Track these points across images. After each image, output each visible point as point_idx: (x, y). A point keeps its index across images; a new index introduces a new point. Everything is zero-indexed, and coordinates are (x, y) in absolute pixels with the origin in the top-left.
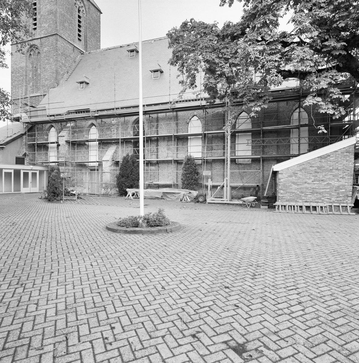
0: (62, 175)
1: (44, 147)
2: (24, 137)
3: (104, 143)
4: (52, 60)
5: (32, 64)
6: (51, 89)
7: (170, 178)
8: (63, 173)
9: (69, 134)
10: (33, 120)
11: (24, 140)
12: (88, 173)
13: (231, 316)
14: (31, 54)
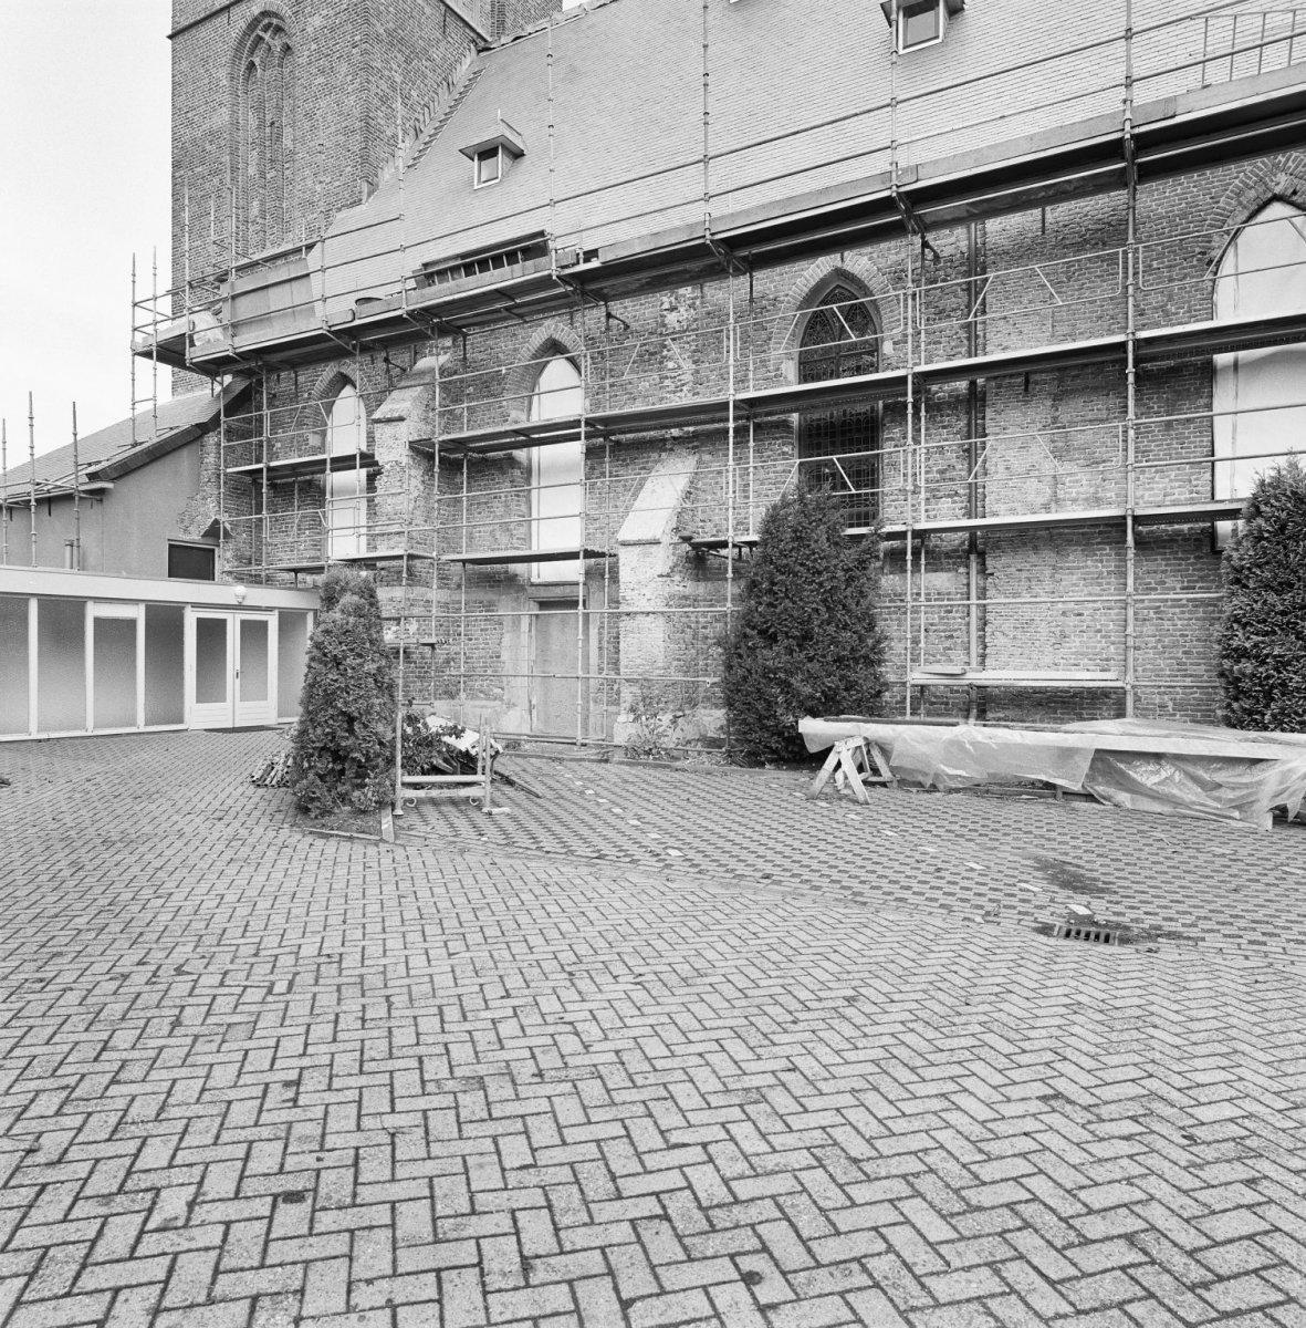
0: (389, 635)
1: (301, 487)
2: (211, 439)
3: (618, 443)
4: (343, 68)
5: (260, 108)
6: (339, 216)
7: (1075, 643)
8: (398, 620)
9: (429, 407)
10: (250, 340)
11: (211, 459)
12: (525, 622)
13: (984, 1184)
14: (252, 66)
